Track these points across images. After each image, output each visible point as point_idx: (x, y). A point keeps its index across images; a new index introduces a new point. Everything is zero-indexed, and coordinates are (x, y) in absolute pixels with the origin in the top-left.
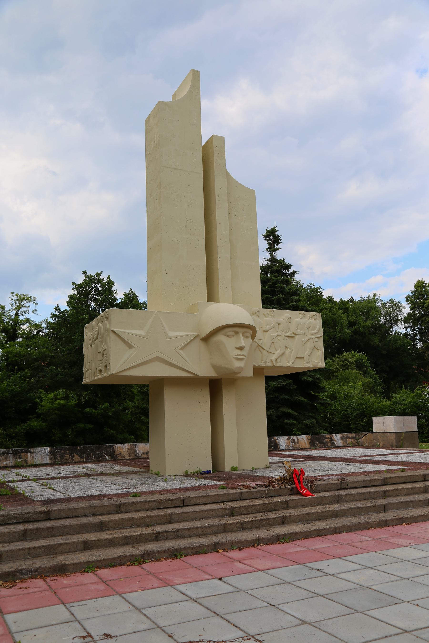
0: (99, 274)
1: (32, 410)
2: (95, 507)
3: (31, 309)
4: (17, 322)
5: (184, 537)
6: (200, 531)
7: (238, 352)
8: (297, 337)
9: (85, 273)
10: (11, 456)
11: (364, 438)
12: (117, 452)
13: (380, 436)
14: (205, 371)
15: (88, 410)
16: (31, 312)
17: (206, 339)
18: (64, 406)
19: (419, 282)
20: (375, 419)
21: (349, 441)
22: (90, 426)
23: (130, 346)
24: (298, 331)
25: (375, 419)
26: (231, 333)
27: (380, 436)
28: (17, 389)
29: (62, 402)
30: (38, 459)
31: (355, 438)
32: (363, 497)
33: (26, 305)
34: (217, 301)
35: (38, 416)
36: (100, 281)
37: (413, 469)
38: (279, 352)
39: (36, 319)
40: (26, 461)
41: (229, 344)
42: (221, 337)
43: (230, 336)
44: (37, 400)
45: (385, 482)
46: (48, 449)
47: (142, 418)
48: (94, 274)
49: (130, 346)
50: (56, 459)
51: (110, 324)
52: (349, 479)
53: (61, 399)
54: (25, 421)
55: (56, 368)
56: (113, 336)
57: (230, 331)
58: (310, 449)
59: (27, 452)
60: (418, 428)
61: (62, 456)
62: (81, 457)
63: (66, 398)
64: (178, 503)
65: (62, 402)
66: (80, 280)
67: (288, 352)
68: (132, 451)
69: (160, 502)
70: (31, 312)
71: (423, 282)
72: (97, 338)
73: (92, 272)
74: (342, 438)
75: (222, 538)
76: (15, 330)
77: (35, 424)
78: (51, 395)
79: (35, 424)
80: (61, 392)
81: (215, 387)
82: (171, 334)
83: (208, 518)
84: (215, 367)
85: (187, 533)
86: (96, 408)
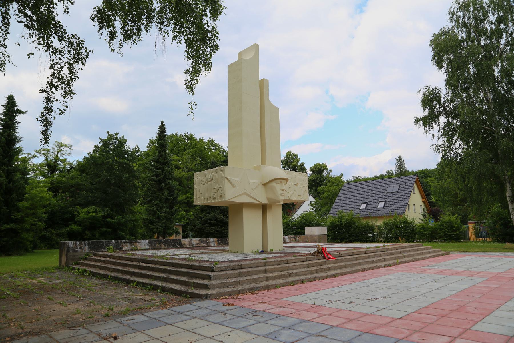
0: (116, 134)
1: (72, 219)
2: (257, 263)
3: (67, 153)
5: (298, 275)
6: (303, 273)
7: (282, 192)
8: (299, 185)
9: (108, 132)
10: (128, 244)
11: (300, 237)
12: (183, 243)
13: (309, 237)
14: (264, 201)
15: (109, 219)
16: (66, 155)
17: (265, 185)
18: (94, 216)
19: (288, 152)
20: (307, 228)
21: (291, 239)
22: (110, 230)
23: (234, 186)
24: (299, 182)
25: (307, 228)
26: (279, 182)
27: (309, 237)
28: (62, 204)
29: (94, 214)
30: (143, 247)
31: (294, 238)
32: (350, 260)
33: (65, 150)
34: (265, 164)
35: (75, 223)
36: (117, 138)
37: (288, 256)
38: (292, 192)
39: (70, 159)
40: (137, 247)
41: (277, 187)
42: (274, 184)
43: (278, 184)
44: (75, 213)
45: (265, 264)
46: (147, 241)
47: (150, 225)
48: (113, 133)
49: (234, 186)
50: (152, 246)
51: (224, 174)
52: (342, 252)
53: (92, 212)
54: (67, 226)
55: (87, 192)
56: (226, 180)
57: (279, 181)
58: (217, 246)
59: (136, 242)
60: (327, 232)
61: (155, 245)
62: (165, 246)
63: (95, 212)
64: (285, 262)
65: (94, 214)
66: (105, 137)
67: (295, 192)
68: (190, 243)
69: (280, 261)
70: (66, 155)
71: (291, 152)
72: (212, 180)
73: (113, 133)
74: (288, 238)
75: (317, 275)
76: (55, 166)
77: (75, 227)
78: (85, 210)
79: (75, 227)
80: (92, 208)
81: (264, 208)
82: (251, 181)
83: (300, 268)
84: (268, 199)
85: (299, 274)
86: (112, 218)
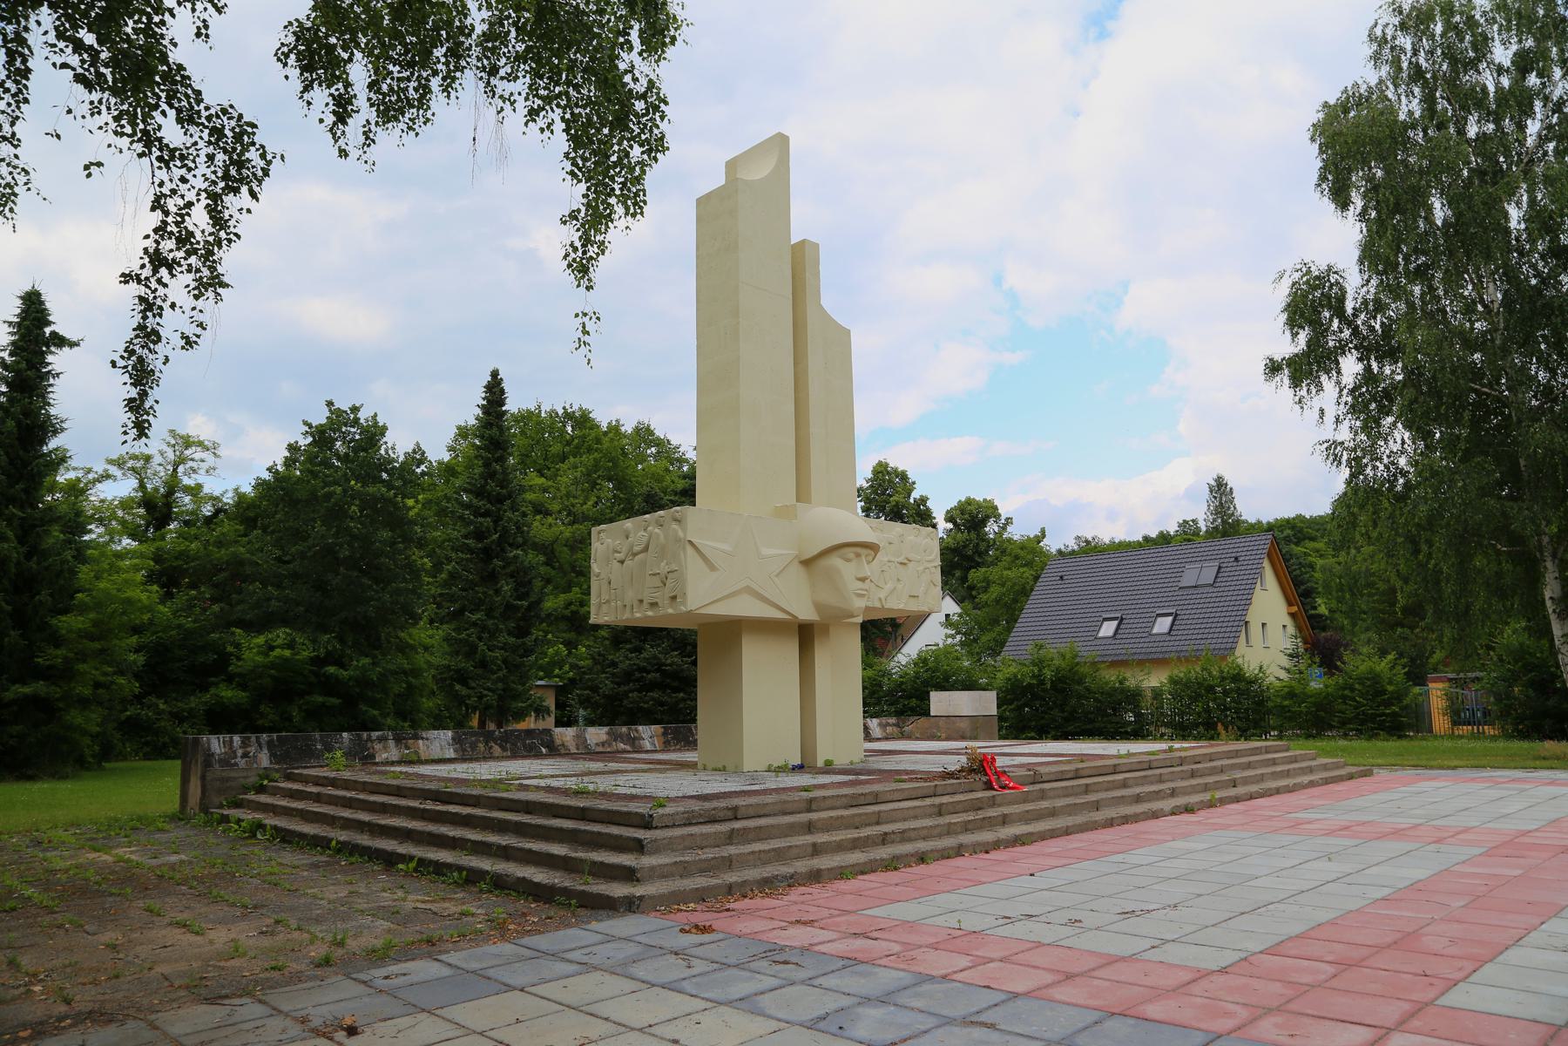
0: (355, 409)
1: (220, 667)
2: (785, 802)
3: (204, 466)
4: (172, 485)
5: (910, 840)
6: (925, 832)
7: (860, 584)
8: (911, 565)
9: (330, 404)
10: (391, 743)
11: (915, 724)
12: (558, 742)
13: (942, 722)
14: (806, 613)
15: (331, 669)
16: (202, 472)
17: (807, 563)
18: (286, 660)
19: (880, 464)
20: (935, 697)
21: (889, 729)
22: (335, 701)
23: (712, 568)
24: (911, 556)
25: (935, 697)
26: (852, 556)
27: (942, 722)
28: (188, 623)
29: (287, 653)
30: (436, 753)
31: (897, 725)
32: (1067, 793)
33: (197, 456)
34: (809, 501)
35: (230, 679)
36: (356, 421)
37: (879, 781)
38: (889, 586)
39: (212, 486)
40: (416, 753)
41: (846, 569)
42: (835, 561)
43: (848, 560)
44: (230, 649)
45: (810, 806)
46: (450, 733)
47: (458, 687)
48: (345, 407)
49: (712, 568)
50: (464, 750)
51: (684, 530)
52: (1043, 770)
53: (282, 647)
54: (204, 688)
55: (265, 586)
56: (689, 549)
57: (850, 552)
58: (662, 751)
59: (416, 737)
60: (999, 707)
61: (474, 746)
62: (504, 749)
63: (291, 645)
64: (870, 799)
65: (287, 653)
66: (320, 417)
67: (900, 586)
68: (581, 740)
69: (853, 796)
70: (202, 472)
71: (887, 465)
72: (646, 549)
73: (344, 405)
74: (880, 724)
75: (967, 839)
76: (168, 506)
77: (229, 694)
78: (261, 640)
79: (229, 694)
80: (281, 634)
81: (806, 635)
82: (766, 551)
83: (916, 817)
84: (818, 607)
85: (913, 834)
86: (342, 666)
